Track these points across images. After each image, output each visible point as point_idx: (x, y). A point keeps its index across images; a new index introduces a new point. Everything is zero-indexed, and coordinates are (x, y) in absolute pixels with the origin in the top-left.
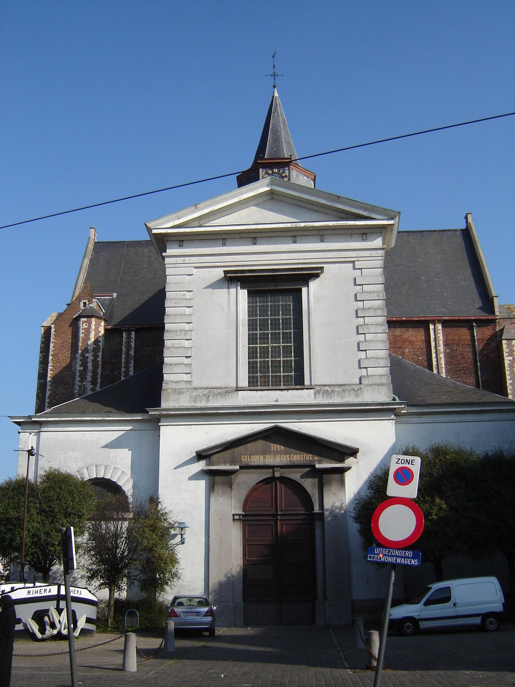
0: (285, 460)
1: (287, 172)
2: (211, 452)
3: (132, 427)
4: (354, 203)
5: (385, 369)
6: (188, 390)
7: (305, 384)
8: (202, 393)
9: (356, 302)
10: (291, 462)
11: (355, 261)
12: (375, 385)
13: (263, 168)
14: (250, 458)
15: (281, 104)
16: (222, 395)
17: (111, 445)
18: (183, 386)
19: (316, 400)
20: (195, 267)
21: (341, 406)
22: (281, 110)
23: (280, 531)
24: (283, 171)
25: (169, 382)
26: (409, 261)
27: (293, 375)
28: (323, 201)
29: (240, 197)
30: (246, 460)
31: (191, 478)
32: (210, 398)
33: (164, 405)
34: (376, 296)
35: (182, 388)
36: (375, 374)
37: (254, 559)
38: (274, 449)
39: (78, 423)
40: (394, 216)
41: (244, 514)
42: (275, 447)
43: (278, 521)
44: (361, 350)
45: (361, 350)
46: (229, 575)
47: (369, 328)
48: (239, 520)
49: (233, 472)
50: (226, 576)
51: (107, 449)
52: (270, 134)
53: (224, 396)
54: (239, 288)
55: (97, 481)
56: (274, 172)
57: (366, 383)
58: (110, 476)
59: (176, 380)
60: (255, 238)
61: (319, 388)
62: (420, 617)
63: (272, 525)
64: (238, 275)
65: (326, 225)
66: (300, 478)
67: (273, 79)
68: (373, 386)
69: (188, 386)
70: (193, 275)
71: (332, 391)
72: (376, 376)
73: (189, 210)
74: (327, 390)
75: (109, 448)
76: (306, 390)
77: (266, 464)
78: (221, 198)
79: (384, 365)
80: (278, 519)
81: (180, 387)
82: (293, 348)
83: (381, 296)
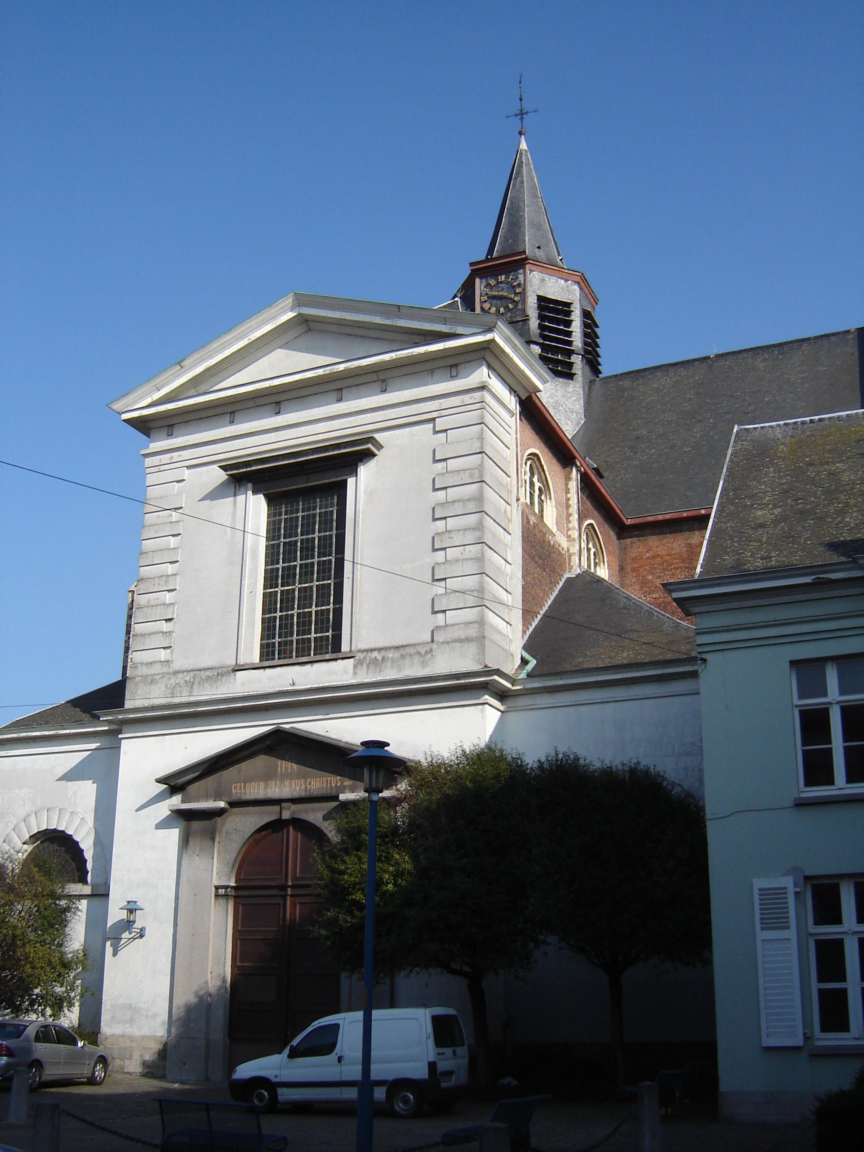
0: (298, 788)
1: (521, 277)
2: (184, 779)
3: (99, 744)
4: (424, 312)
5: (476, 611)
6: (163, 675)
7: (343, 650)
8: (183, 679)
9: (435, 493)
10: (306, 791)
11: (435, 418)
12: (456, 642)
13: (481, 278)
14: (244, 788)
15: (531, 162)
16: (212, 680)
17: (71, 776)
18: (157, 669)
19: (357, 677)
20: (188, 467)
21: (388, 685)
22: (529, 171)
23: (290, 916)
24: (514, 278)
25: (139, 665)
26: (746, 403)
27: (330, 636)
28: (378, 320)
29: (250, 337)
30: (238, 791)
31: (159, 826)
32: (194, 687)
33: (128, 704)
34: (467, 477)
35: (157, 673)
36: (458, 622)
37: (249, 964)
38: (281, 769)
39: (29, 742)
40: (493, 325)
41: (236, 886)
42: (284, 766)
43: (289, 897)
44: (438, 580)
45: (438, 580)
46: (202, 993)
47: (453, 537)
48: (226, 896)
49: (220, 812)
50: (196, 994)
51: (64, 782)
52: (506, 216)
53: (215, 681)
54: (250, 493)
55: (54, 835)
56: (499, 280)
57: (441, 640)
58: (64, 826)
59: (149, 661)
60: (278, 403)
61: (360, 656)
62: (278, 1080)
63: (279, 904)
64: (241, 470)
65: (379, 361)
66: (322, 819)
67: (520, 122)
68: (453, 644)
69: (165, 670)
70: (184, 480)
71: (383, 658)
72: (459, 624)
73: (172, 373)
74: (376, 657)
75: (67, 781)
76: (341, 661)
77: (268, 797)
78: (218, 344)
79: (159, 695)
80: (288, 895)
81: (153, 672)
82: (332, 588)
83: (476, 476)
